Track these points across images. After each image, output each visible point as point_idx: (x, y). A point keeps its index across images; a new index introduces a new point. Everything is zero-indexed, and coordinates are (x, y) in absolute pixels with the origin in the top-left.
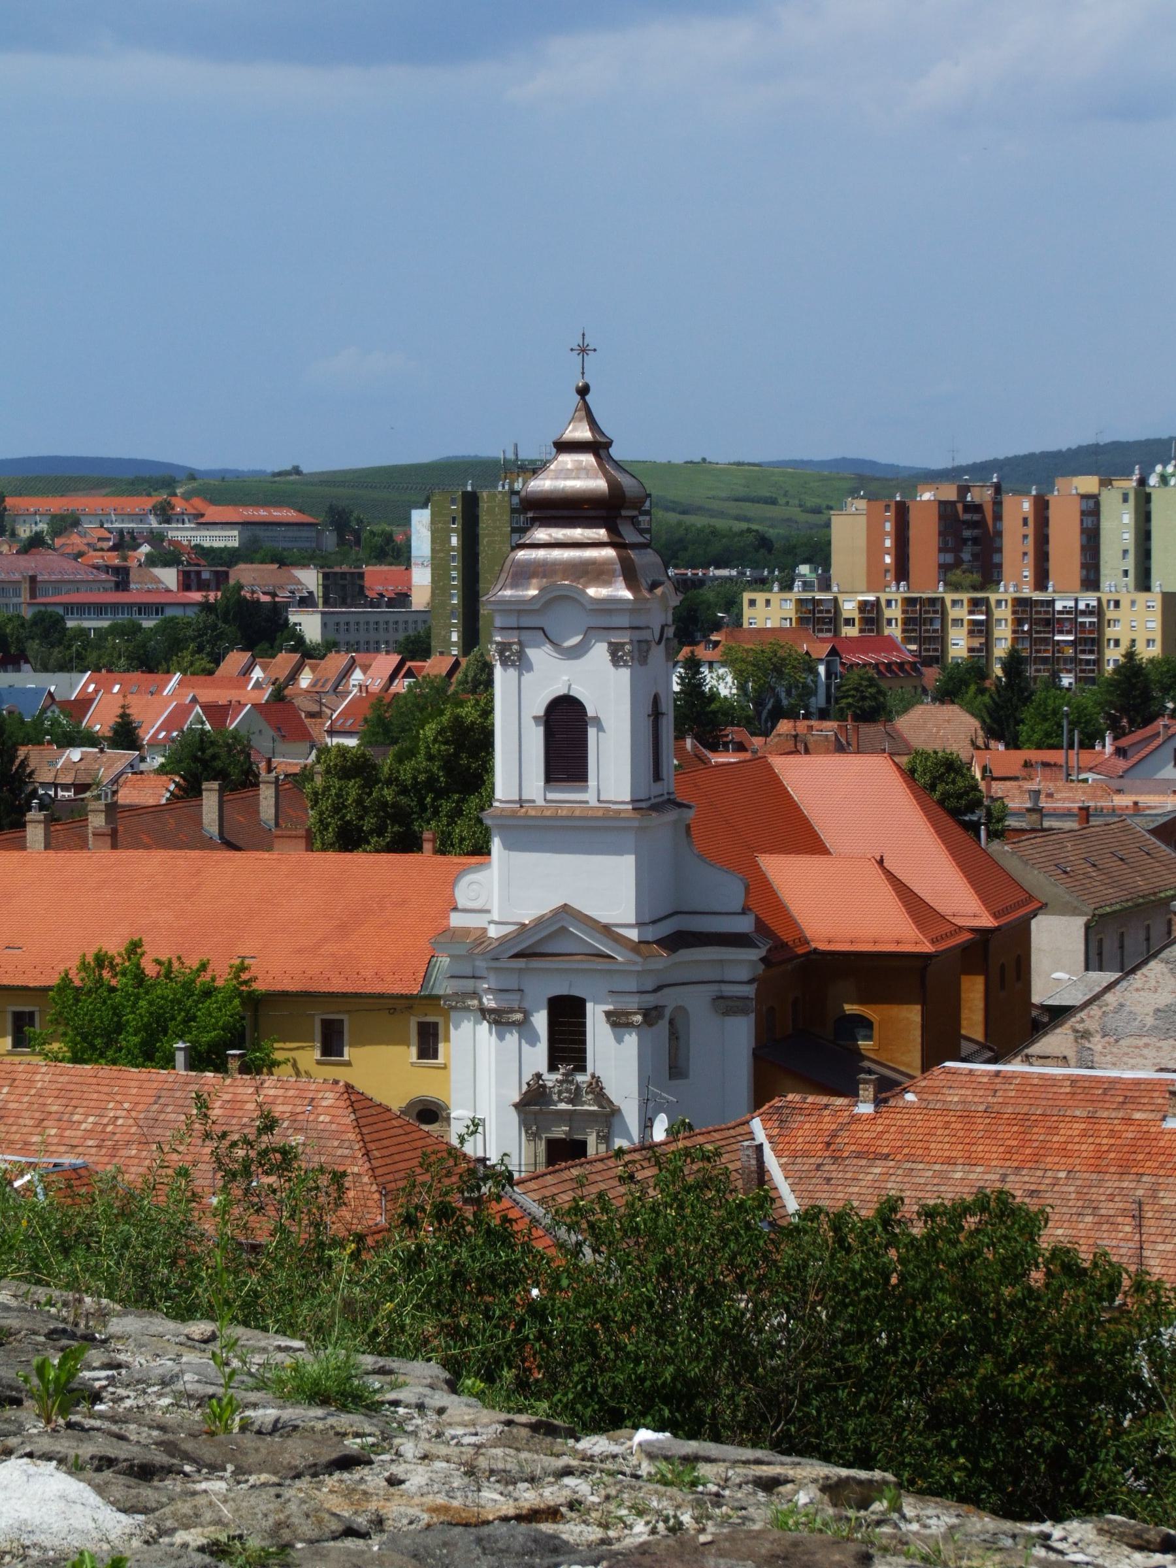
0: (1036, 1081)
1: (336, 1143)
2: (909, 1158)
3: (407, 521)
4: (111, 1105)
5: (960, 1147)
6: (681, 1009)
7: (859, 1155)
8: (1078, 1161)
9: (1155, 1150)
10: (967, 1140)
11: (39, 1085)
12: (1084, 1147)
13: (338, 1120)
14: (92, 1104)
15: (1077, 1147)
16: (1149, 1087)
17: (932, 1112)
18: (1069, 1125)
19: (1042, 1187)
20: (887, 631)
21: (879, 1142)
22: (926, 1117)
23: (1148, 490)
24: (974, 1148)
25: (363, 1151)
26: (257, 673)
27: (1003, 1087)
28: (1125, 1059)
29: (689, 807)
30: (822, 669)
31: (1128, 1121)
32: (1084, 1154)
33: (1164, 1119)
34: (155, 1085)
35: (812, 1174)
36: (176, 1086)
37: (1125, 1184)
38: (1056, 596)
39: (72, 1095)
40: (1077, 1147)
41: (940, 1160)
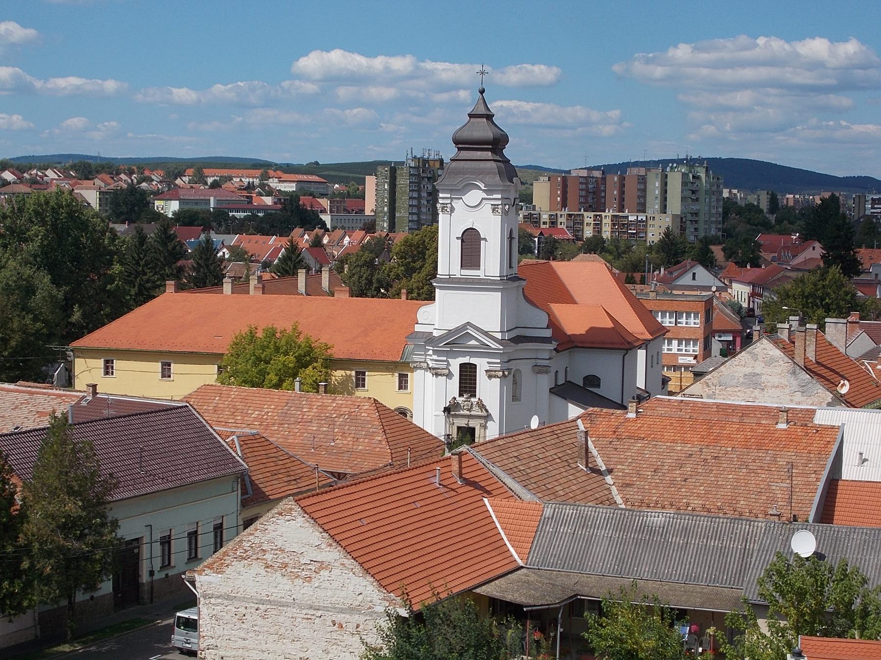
0: (700, 405)
1: (370, 426)
2: (654, 439)
3: (363, 182)
4: (266, 406)
5: (679, 435)
6: (518, 370)
7: (630, 438)
8: (737, 443)
9: (773, 439)
10: (682, 432)
11: (233, 396)
12: (739, 436)
13: (370, 415)
14: (257, 405)
15: (735, 436)
16: (754, 409)
17: (664, 418)
18: (731, 426)
19: (720, 455)
20: (559, 226)
21: (639, 432)
22: (661, 420)
23: (666, 173)
24: (685, 436)
25: (383, 430)
26: (306, 237)
27: (685, 408)
28: (729, 397)
29: (525, 280)
30: (536, 239)
31: (759, 424)
32: (739, 440)
33: (777, 423)
34: (286, 398)
35: (608, 446)
36: (296, 398)
37: (761, 454)
38: (629, 214)
39: (248, 401)
40: (735, 436)
41: (670, 441)
